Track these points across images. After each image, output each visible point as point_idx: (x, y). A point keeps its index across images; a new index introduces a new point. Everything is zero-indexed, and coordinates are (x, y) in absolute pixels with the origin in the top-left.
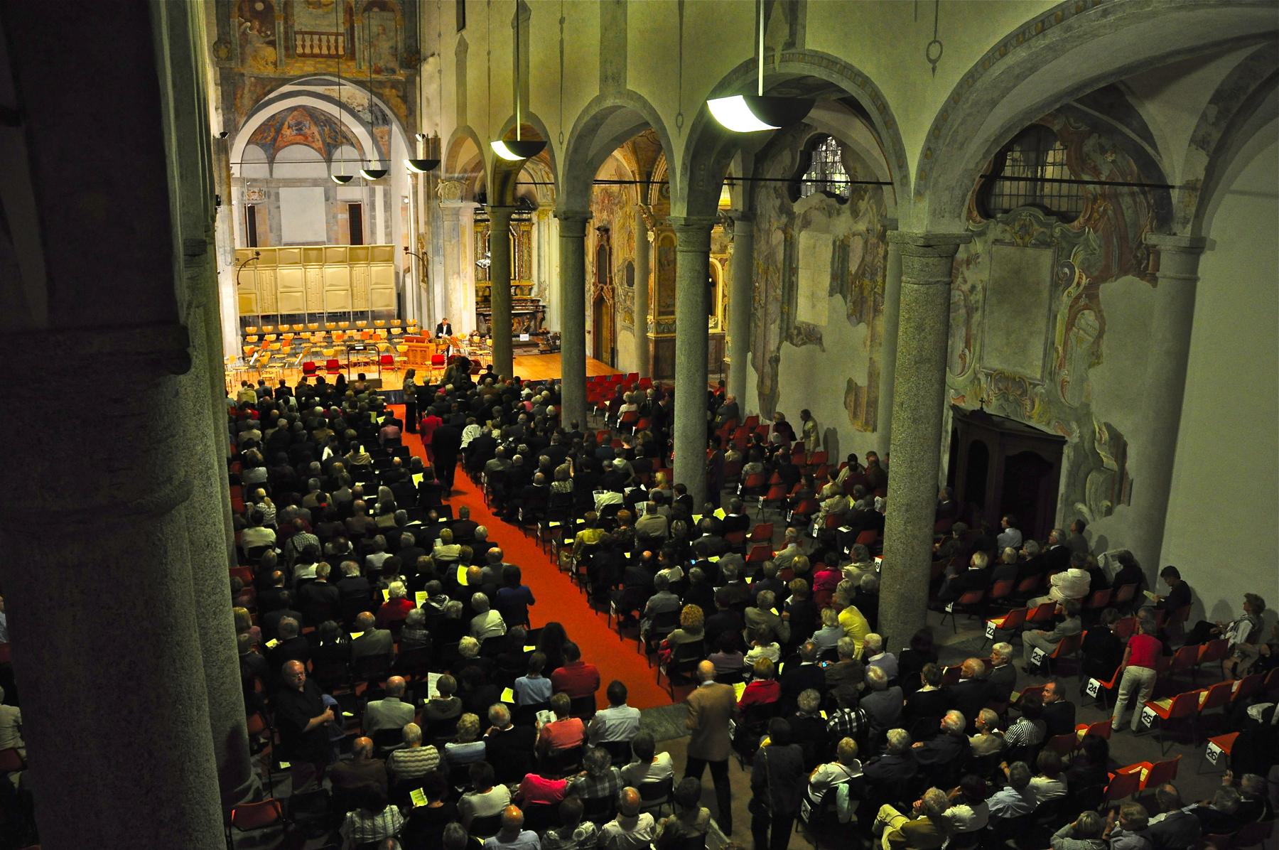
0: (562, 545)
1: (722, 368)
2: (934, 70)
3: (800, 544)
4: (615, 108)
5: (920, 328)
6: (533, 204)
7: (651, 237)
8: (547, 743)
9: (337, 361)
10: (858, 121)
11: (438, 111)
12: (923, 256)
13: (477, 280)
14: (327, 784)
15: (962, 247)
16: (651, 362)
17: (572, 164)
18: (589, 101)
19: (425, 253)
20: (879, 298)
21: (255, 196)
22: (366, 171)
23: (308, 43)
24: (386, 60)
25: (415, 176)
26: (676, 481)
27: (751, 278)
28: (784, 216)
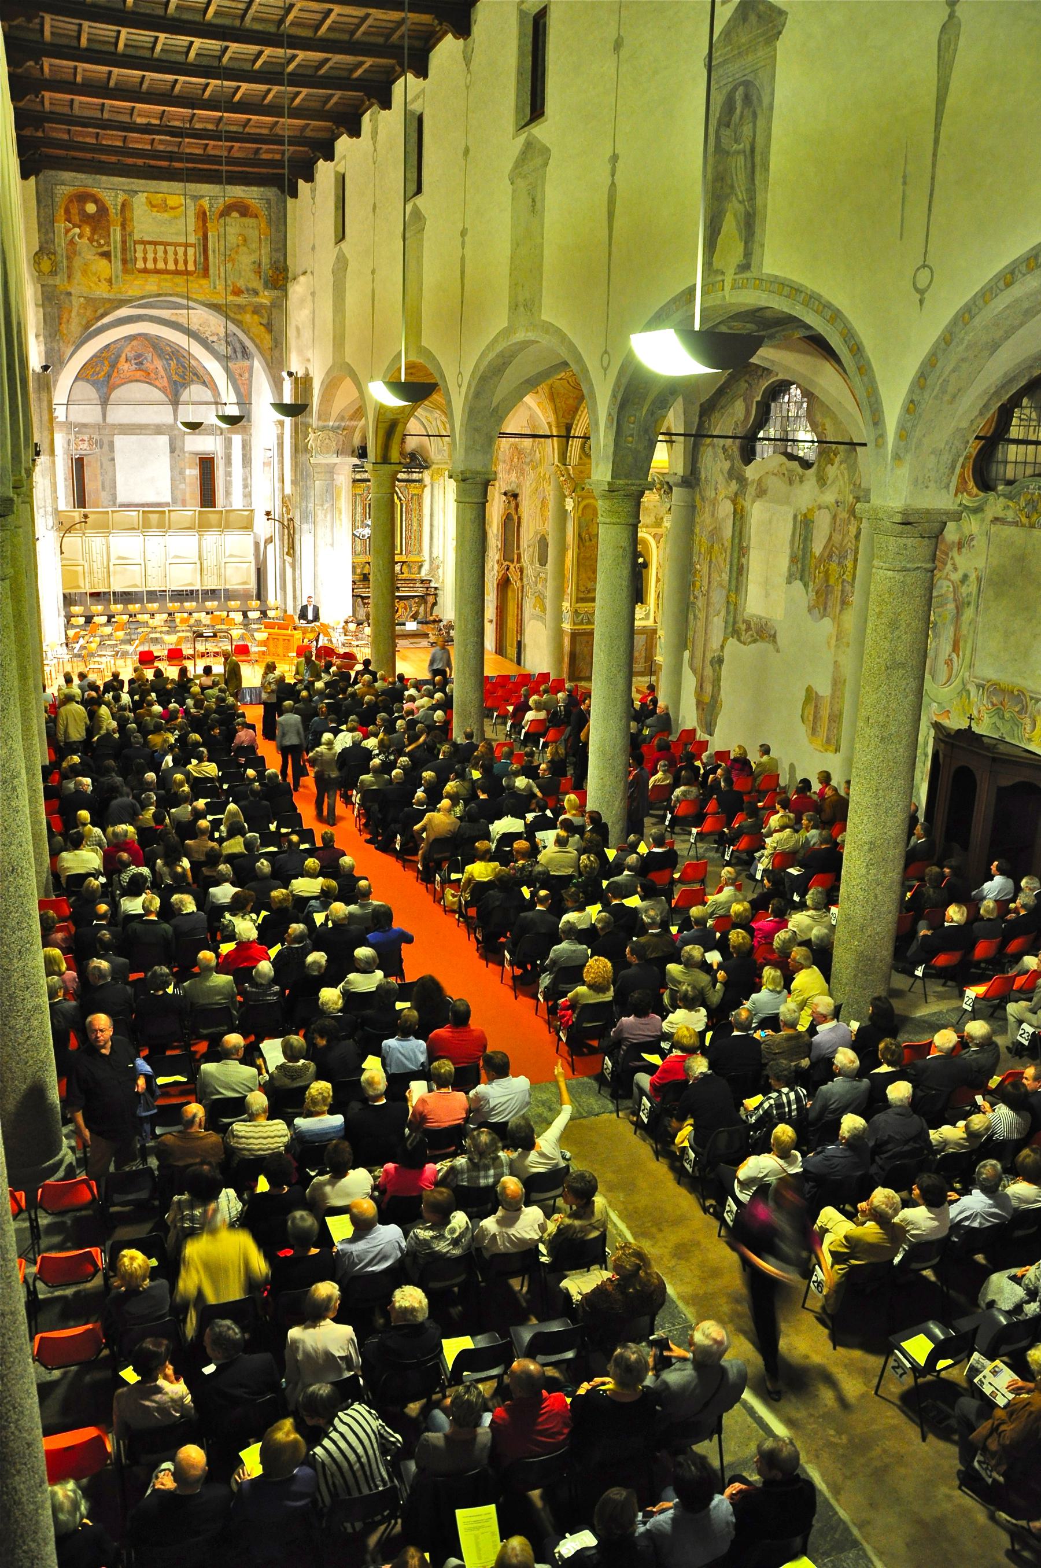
0: (447, 882)
1: (651, 669)
2: (921, 302)
3: (739, 888)
4: (525, 344)
5: (893, 625)
6: (425, 461)
7: (569, 503)
8: (421, 1117)
9: (180, 650)
10: (828, 364)
11: (310, 343)
12: (900, 535)
13: (354, 553)
14: (153, 1162)
15: (951, 526)
16: (566, 660)
17: (472, 413)
18: (495, 334)
19: (291, 519)
20: (848, 588)
21: (85, 446)
22: (218, 416)
23: (150, 256)
24: (248, 279)
25: (281, 424)
26: (589, 807)
27: (691, 558)
28: (734, 482)
